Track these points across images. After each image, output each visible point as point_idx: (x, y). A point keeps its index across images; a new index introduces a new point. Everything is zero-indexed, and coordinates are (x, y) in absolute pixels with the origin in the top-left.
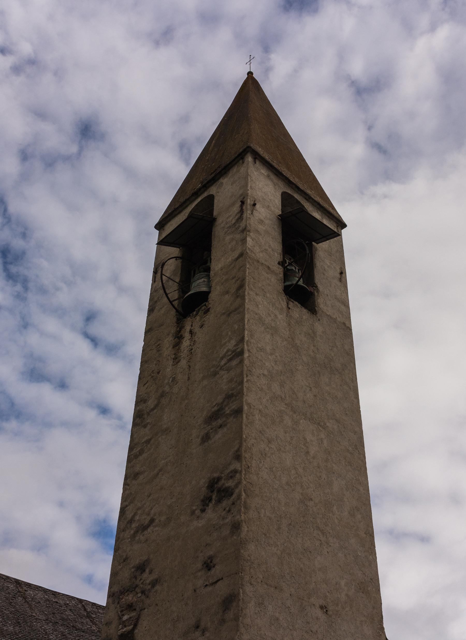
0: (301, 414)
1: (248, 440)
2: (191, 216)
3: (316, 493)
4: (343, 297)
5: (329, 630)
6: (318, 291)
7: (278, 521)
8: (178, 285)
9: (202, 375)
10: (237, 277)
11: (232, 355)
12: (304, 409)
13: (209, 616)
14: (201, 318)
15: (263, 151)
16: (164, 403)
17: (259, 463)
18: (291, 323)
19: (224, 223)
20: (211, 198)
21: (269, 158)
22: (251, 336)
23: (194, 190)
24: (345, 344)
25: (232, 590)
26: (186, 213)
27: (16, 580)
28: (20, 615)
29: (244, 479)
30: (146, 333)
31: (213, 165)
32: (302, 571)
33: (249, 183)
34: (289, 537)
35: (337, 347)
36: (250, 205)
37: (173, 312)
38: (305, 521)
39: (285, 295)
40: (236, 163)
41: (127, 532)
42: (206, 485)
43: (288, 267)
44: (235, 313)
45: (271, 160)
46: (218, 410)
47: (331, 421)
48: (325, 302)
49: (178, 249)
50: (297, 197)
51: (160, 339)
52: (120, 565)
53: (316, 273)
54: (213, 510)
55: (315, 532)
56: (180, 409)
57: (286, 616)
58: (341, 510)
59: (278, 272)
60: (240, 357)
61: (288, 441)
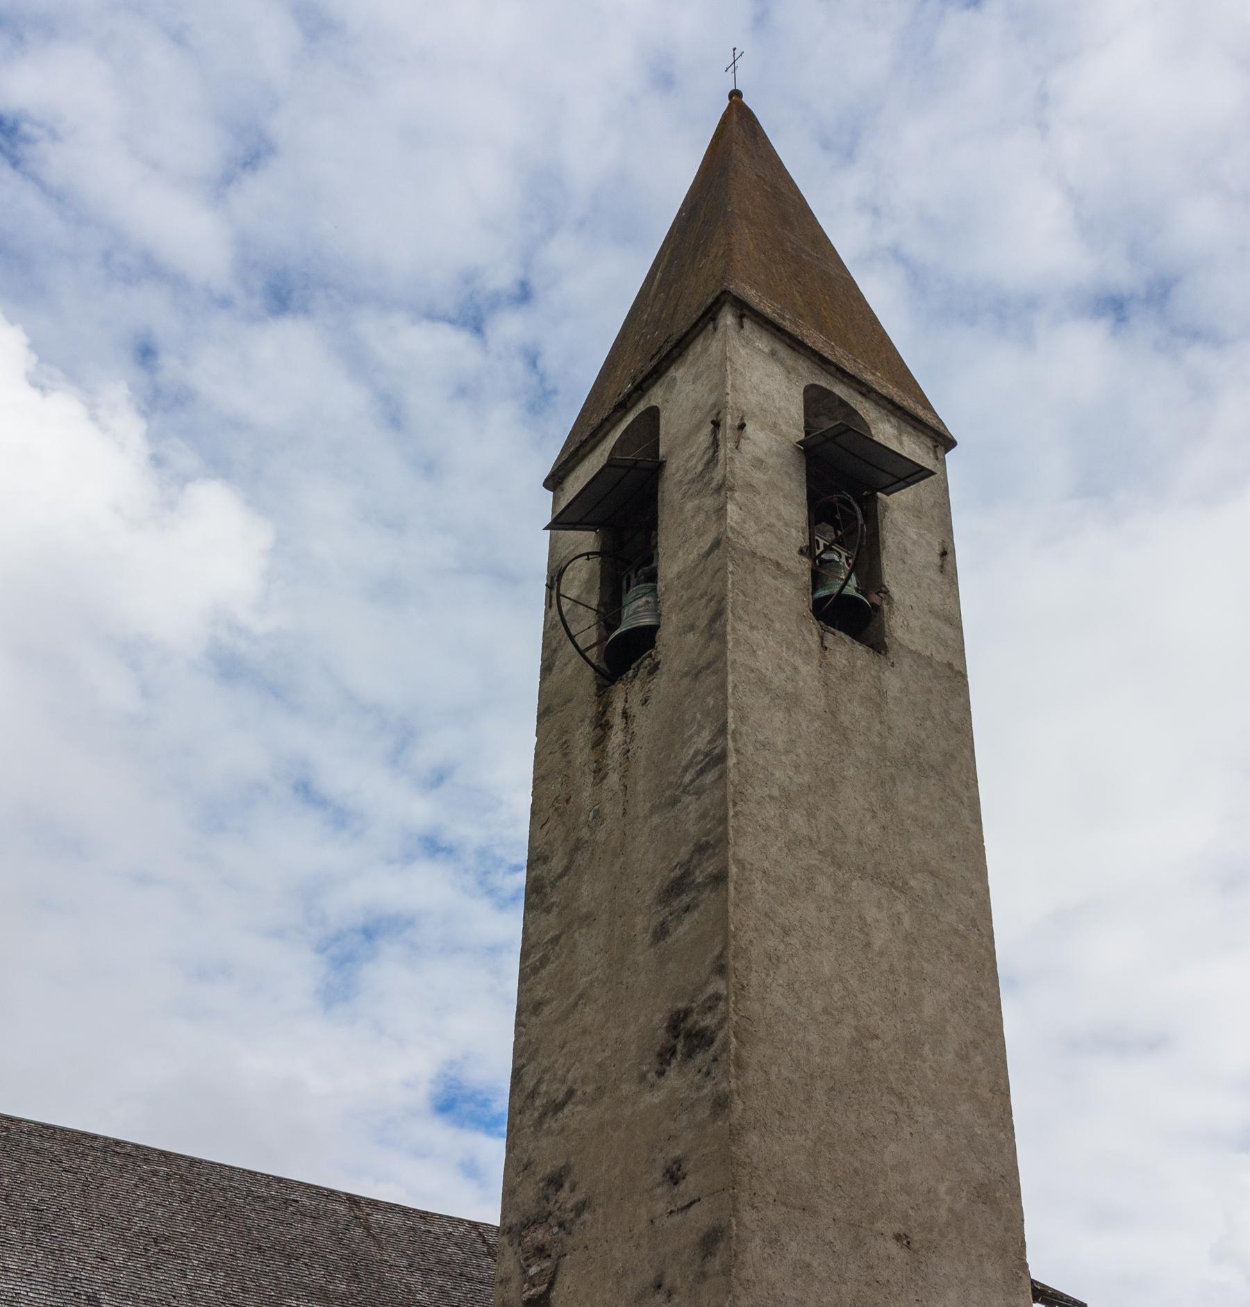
0: (852, 869)
1: (741, 934)
2: (610, 464)
3: (887, 1023)
4: (947, 607)
5: (913, 1276)
6: (890, 601)
7: (806, 1085)
8: (595, 613)
9: (649, 805)
10: (710, 594)
11: (704, 762)
12: (860, 857)
13: (678, 1267)
14: (644, 683)
15: (760, 294)
16: (581, 862)
17: (764, 976)
18: (830, 679)
19: (681, 473)
20: (653, 414)
21: (774, 311)
22: (741, 721)
23: (618, 396)
24: (952, 709)
25: (718, 1219)
26: (604, 450)
27: (348, 1196)
28: (359, 1262)
29: (733, 1012)
30: (540, 717)
31: (655, 335)
32: (857, 1175)
33: (730, 377)
34: (831, 1113)
35: (933, 717)
36: (732, 428)
37: (589, 672)
38: (864, 1079)
39: (816, 621)
40: (701, 331)
41: (528, 1115)
42: (665, 1025)
43: (823, 556)
44: (709, 671)
45: (777, 314)
46: (683, 876)
47: (919, 876)
48: (906, 623)
49: (594, 534)
50: (841, 391)
51: (567, 731)
52: (517, 1175)
53: (885, 562)
54: (679, 1072)
55: (884, 1098)
56: (611, 875)
57: (826, 1259)
58: (940, 1051)
59: (799, 571)
60: (719, 767)
61: (826, 926)
